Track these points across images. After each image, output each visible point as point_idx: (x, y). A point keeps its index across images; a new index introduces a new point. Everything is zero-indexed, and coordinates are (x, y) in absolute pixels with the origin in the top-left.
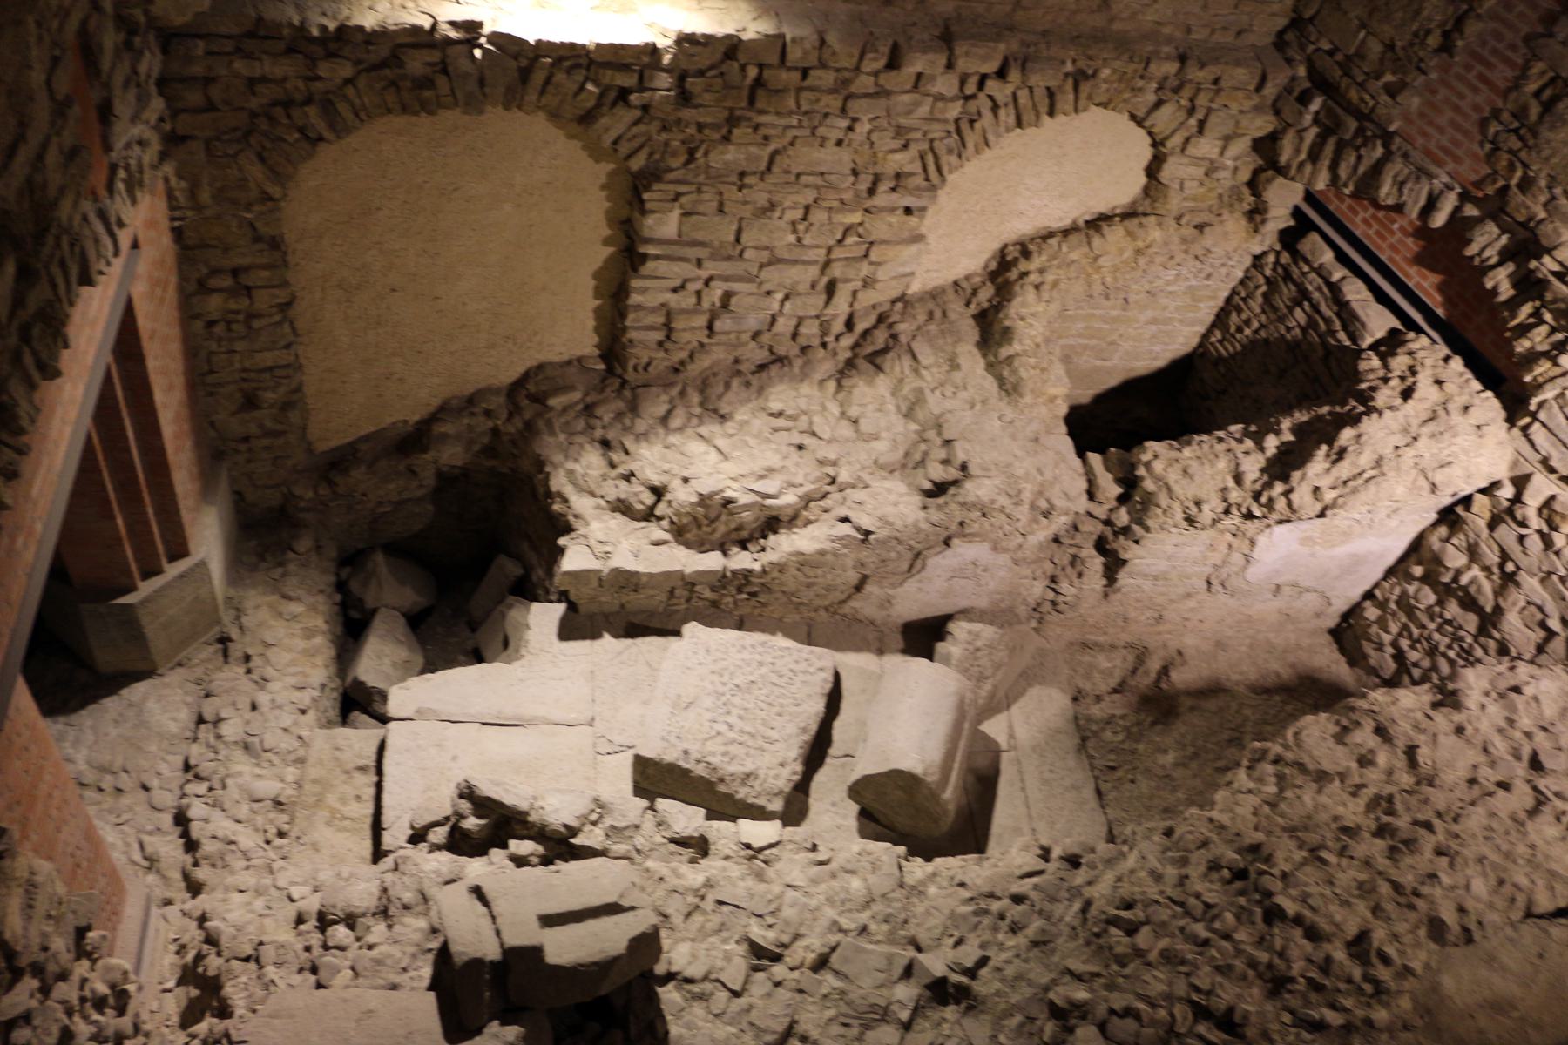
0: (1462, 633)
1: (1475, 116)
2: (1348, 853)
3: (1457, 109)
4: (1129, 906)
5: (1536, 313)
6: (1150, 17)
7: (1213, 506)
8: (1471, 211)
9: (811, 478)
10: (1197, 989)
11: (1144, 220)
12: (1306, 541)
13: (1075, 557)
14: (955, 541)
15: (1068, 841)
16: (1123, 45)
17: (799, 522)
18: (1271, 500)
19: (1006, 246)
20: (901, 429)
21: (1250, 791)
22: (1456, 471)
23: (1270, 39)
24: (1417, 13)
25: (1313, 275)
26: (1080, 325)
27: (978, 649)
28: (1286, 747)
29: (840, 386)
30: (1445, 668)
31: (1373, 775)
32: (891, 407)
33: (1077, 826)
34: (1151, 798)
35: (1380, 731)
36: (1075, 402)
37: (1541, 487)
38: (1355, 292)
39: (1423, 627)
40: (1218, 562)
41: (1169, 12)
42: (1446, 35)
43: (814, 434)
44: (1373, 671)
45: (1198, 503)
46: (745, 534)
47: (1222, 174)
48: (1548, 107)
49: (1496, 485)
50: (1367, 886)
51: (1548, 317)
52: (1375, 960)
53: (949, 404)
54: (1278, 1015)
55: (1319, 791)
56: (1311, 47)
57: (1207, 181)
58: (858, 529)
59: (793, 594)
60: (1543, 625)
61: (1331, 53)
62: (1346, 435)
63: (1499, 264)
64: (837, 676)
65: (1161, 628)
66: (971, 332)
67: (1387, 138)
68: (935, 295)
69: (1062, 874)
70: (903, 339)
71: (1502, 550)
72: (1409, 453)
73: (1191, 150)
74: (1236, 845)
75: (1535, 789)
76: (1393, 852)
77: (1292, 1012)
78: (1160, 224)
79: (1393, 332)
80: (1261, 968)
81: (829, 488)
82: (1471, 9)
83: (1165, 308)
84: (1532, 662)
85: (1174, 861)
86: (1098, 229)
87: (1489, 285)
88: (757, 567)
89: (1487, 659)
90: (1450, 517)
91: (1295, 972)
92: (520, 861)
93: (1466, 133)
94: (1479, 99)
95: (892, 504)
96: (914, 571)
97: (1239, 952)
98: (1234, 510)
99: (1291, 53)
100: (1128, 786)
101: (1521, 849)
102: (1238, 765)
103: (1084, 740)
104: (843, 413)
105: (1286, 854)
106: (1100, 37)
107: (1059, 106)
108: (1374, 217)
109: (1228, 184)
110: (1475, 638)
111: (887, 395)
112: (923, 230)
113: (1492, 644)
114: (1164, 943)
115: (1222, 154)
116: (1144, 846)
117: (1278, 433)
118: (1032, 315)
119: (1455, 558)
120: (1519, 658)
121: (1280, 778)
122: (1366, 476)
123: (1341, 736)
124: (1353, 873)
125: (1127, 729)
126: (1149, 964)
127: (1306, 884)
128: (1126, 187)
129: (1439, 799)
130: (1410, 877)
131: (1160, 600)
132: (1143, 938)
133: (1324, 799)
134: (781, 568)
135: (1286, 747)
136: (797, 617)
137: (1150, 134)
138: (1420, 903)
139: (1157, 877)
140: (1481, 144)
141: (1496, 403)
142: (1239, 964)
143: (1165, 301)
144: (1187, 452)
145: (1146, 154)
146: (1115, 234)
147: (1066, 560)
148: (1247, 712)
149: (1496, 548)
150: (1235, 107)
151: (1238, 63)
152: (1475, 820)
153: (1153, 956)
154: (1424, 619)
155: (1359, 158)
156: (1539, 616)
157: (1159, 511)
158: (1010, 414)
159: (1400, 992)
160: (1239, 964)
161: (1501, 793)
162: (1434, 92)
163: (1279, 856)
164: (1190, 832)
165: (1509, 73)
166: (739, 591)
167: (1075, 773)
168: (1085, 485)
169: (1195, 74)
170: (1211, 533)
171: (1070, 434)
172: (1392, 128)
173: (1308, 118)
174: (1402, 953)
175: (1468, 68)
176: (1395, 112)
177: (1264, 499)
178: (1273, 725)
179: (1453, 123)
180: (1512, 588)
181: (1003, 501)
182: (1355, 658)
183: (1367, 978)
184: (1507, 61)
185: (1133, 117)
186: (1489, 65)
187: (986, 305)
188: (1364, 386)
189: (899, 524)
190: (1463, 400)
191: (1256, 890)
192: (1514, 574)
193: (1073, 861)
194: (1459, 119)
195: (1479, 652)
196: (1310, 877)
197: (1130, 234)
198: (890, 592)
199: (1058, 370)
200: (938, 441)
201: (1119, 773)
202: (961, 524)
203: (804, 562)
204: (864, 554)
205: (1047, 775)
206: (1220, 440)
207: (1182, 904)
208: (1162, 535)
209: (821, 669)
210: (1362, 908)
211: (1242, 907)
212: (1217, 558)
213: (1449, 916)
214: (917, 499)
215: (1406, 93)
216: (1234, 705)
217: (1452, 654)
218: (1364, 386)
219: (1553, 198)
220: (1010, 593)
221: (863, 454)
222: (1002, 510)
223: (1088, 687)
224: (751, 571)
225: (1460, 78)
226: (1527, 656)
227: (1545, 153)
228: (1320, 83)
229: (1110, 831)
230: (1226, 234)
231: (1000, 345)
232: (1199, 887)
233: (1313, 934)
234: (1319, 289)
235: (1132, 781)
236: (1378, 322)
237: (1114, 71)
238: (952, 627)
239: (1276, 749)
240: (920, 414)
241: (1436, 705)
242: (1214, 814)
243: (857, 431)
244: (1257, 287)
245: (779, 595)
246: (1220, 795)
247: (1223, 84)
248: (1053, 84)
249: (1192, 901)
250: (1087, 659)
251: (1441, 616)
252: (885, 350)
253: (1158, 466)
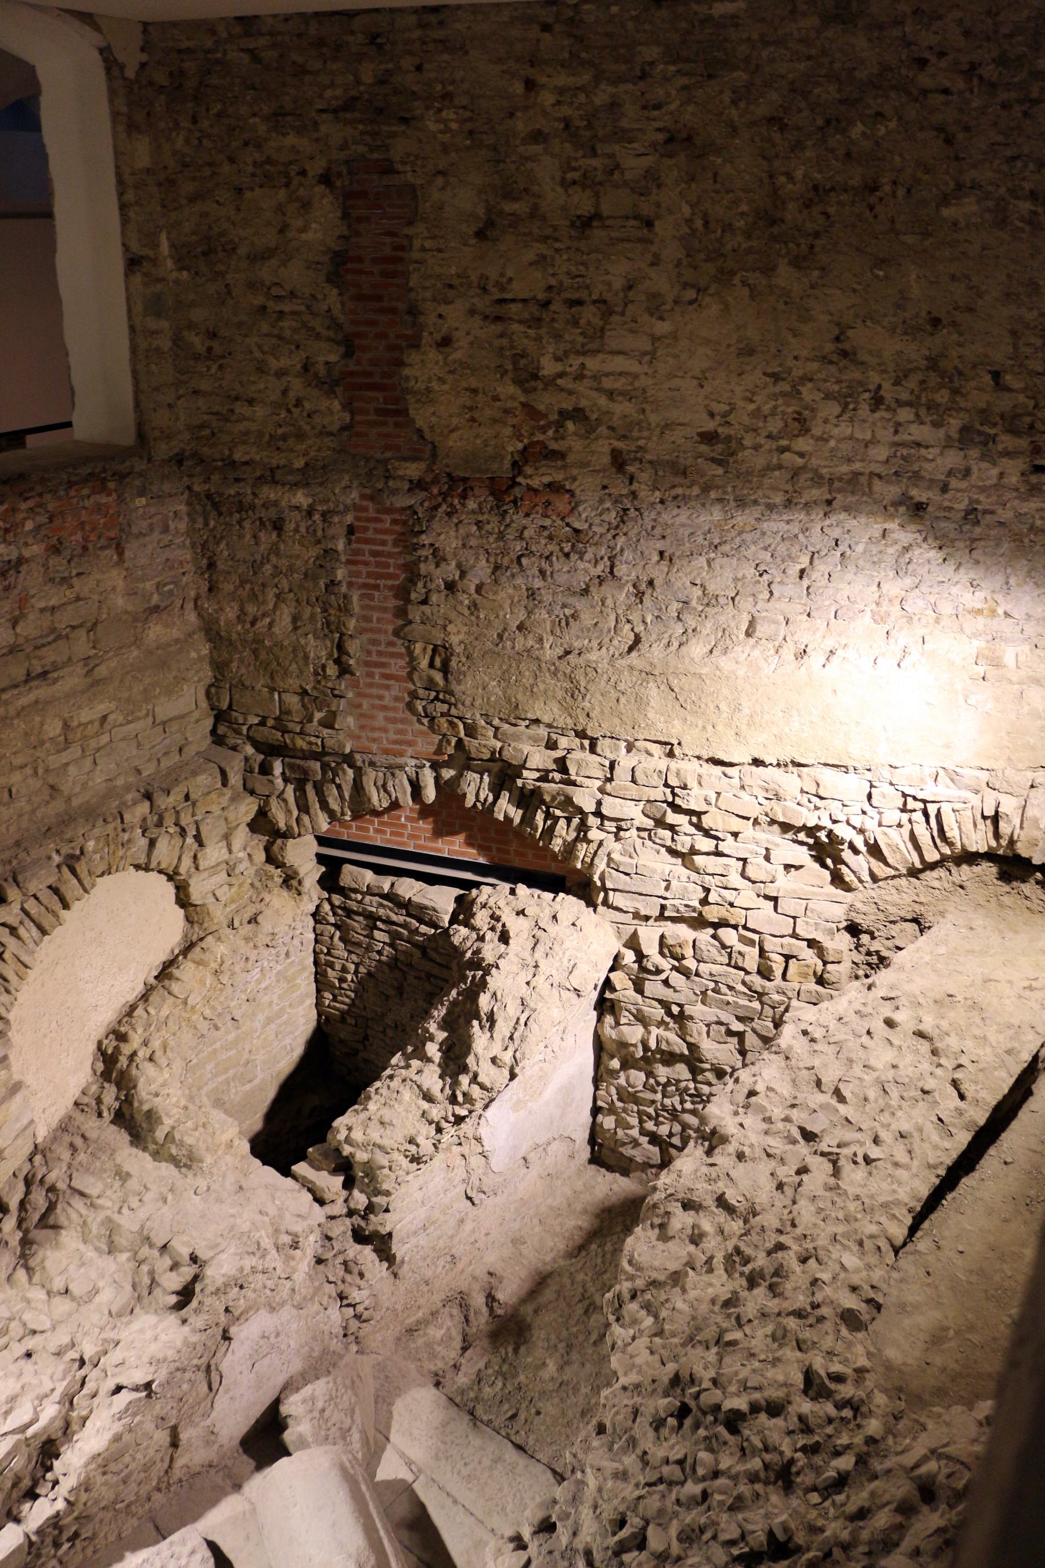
0: (683, 1085)
1: (401, 705)
2: (744, 1320)
3: (384, 708)
4: (622, 1523)
5: (548, 815)
6: (99, 779)
7: (425, 1134)
8: (448, 774)
9: (59, 1373)
10: (732, 1543)
11: (203, 944)
12: (517, 1106)
13: (345, 1263)
14: (233, 1330)
15: (528, 1513)
16: (91, 814)
17: (75, 1427)
18: (464, 1094)
19: (100, 1043)
20: (113, 1267)
21: (634, 1338)
22: (583, 968)
23: (209, 740)
24: (306, 657)
25: (368, 898)
26: (210, 1067)
27: (323, 1410)
28: (631, 1278)
29: (29, 1270)
30: (693, 1121)
31: (711, 1243)
32: (90, 1254)
33: (526, 1493)
34: (563, 1414)
35: (688, 1205)
36: (252, 1134)
37: (649, 937)
38: (409, 889)
39: (653, 1102)
40: (465, 1176)
41: (113, 766)
42: (337, 661)
43: (34, 1332)
44: (646, 1166)
45: (412, 1141)
46: (27, 1483)
47: (241, 867)
48: (445, 670)
49: (617, 958)
50: (779, 1333)
51: (558, 813)
52: (832, 1386)
53: (142, 1214)
54: (807, 1502)
55: (684, 1291)
56: (244, 729)
57: (233, 880)
58: (136, 1389)
59: (115, 1503)
60: (730, 1033)
61: (263, 723)
62: (484, 1001)
63: (496, 798)
64: (213, 1546)
65: (460, 1266)
66: (120, 1137)
67: (348, 759)
68: (64, 1127)
69: (546, 1547)
70: (61, 1186)
71: (660, 1001)
72: (540, 981)
73: (202, 864)
74: (660, 1391)
75: (823, 1154)
76: (773, 1290)
77: (815, 1489)
78: (219, 939)
79: (459, 900)
80: (762, 1475)
81: (83, 1372)
82: (342, 635)
83: (270, 1004)
84: (744, 1065)
85: (624, 1450)
86: (170, 976)
87: (501, 818)
88: (60, 1505)
89: (714, 1090)
90: (605, 1006)
91: (788, 1454)
93: (403, 721)
94: (394, 692)
95: (153, 1341)
96: (215, 1386)
97: (735, 1478)
98: (444, 1125)
99: (231, 741)
100: (537, 1420)
101: (852, 1206)
102: (608, 1325)
103: (471, 1413)
104: (49, 1293)
105: (701, 1363)
106: (67, 820)
107: (68, 896)
108: (381, 823)
109: (252, 871)
110: (694, 1080)
111: (82, 1247)
112: (16, 1077)
113: (710, 1076)
114: (673, 1531)
115: (230, 852)
116: (590, 1459)
117: (431, 1039)
118: (163, 1085)
119: (634, 1034)
120: (734, 1070)
121: (647, 1307)
122: (522, 1021)
123: (664, 1235)
124: (760, 1333)
125: (499, 1373)
126: (679, 1559)
127: (736, 1373)
128: (172, 926)
129: (770, 1220)
130: (801, 1298)
131: (441, 1243)
132: (655, 1541)
133: (692, 1294)
134: (86, 1486)
135: (631, 1278)
136: (135, 1522)
137: (160, 872)
138: (825, 1311)
139: (622, 1476)
140: (420, 722)
141: (571, 898)
142: (744, 1488)
143: (266, 999)
144: (372, 1106)
145: (170, 889)
146: (187, 971)
147: (340, 1271)
148: (581, 1277)
149: (655, 1004)
150: (216, 809)
151: (195, 774)
152: (805, 1212)
153: (676, 1549)
154: (648, 1096)
155: (339, 787)
156: (723, 1029)
157: (386, 1171)
158: (202, 1183)
159: (869, 1395)
160: (744, 1488)
161: (805, 1177)
162: (360, 706)
163: (698, 1370)
164: (617, 1413)
165: (402, 663)
166: (57, 1545)
167: (487, 1449)
168: (310, 1197)
169: (164, 802)
170: (439, 1157)
171: (265, 1163)
172: (347, 751)
173: (279, 782)
174: (845, 1362)
175: (370, 675)
176: (341, 736)
177: (460, 1099)
178: (608, 1269)
179: (387, 719)
180: (689, 1024)
181: (249, 1262)
182: (624, 1167)
183: (839, 1406)
184: (393, 655)
185: (137, 867)
186: (383, 665)
187: (117, 1105)
188: (468, 955)
189: (171, 1354)
190: (547, 914)
191: (705, 1414)
192: (682, 1012)
193: (547, 1527)
194: (391, 714)
195: (706, 1090)
196: (734, 1366)
197: (199, 963)
198: (208, 1422)
199: (217, 1116)
200: (156, 1253)
201: (522, 1416)
202: (227, 1310)
203: (104, 1462)
204: (158, 1407)
205: (465, 1471)
206: (391, 1077)
207: (661, 1480)
208: (403, 1189)
209: (193, 1552)
210: (790, 1353)
211: (706, 1438)
212: (460, 1173)
213: (850, 1302)
214: (173, 1319)
215: (339, 719)
216: (566, 1280)
217: (688, 1106)
218: (468, 955)
219: (497, 729)
220: (314, 1338)
221: (93, 1316)
222: (254, 1270)
223: (440, 1364)
224: (57, 1515)
225: (371, 685)
226: (739, 1064)
227: (468, 703)
228: (270, 750)
229: (554, 1472)
230: (277, 911)
231: (152, 1131)
232: (661, 1453)
233: (775, 1409)
234: (381, 905)
235: (538, 1413)
236: (442, 900)
237: (98, 839)
238: (284, 1409)
239: (624, 1287)
240: (122, 1241)
241: (709, 1153)
242: (623, 1381)
243: (73, 1299)
244: (332, 938)
245: (101, 1515)
246: (615, 1362)
247: (193, 796)
248: (52, 880)
249: (666, 1470)
250: (420, 1342)
251: (658, 1084)
252: (51, 1207)
253: (357, 1135)
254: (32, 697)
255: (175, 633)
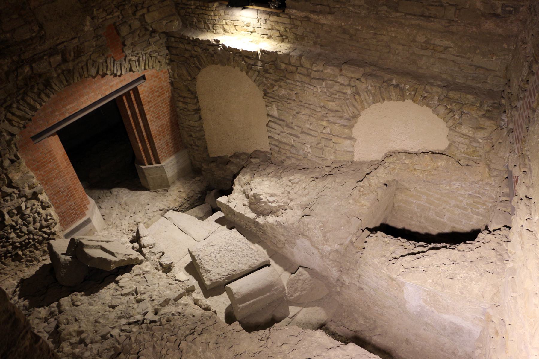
92: (133, 248)
209: (257, 260)
254: (417, 22)
255: (500, 31)
